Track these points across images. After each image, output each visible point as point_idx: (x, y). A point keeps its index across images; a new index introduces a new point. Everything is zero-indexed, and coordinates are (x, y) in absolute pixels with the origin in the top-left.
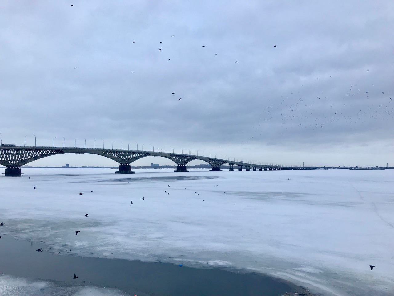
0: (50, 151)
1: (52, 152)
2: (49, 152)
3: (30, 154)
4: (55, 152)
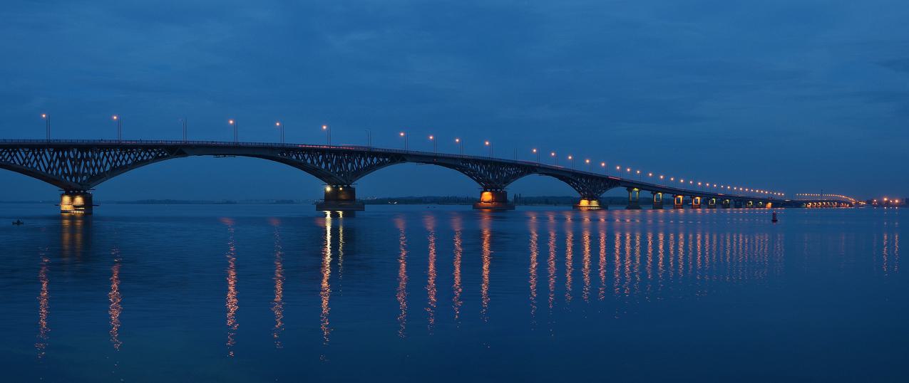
0: (155, 152)
1: (160, 155)
2: (153, 154)
3: (111, 159)
4: (166, 154)
